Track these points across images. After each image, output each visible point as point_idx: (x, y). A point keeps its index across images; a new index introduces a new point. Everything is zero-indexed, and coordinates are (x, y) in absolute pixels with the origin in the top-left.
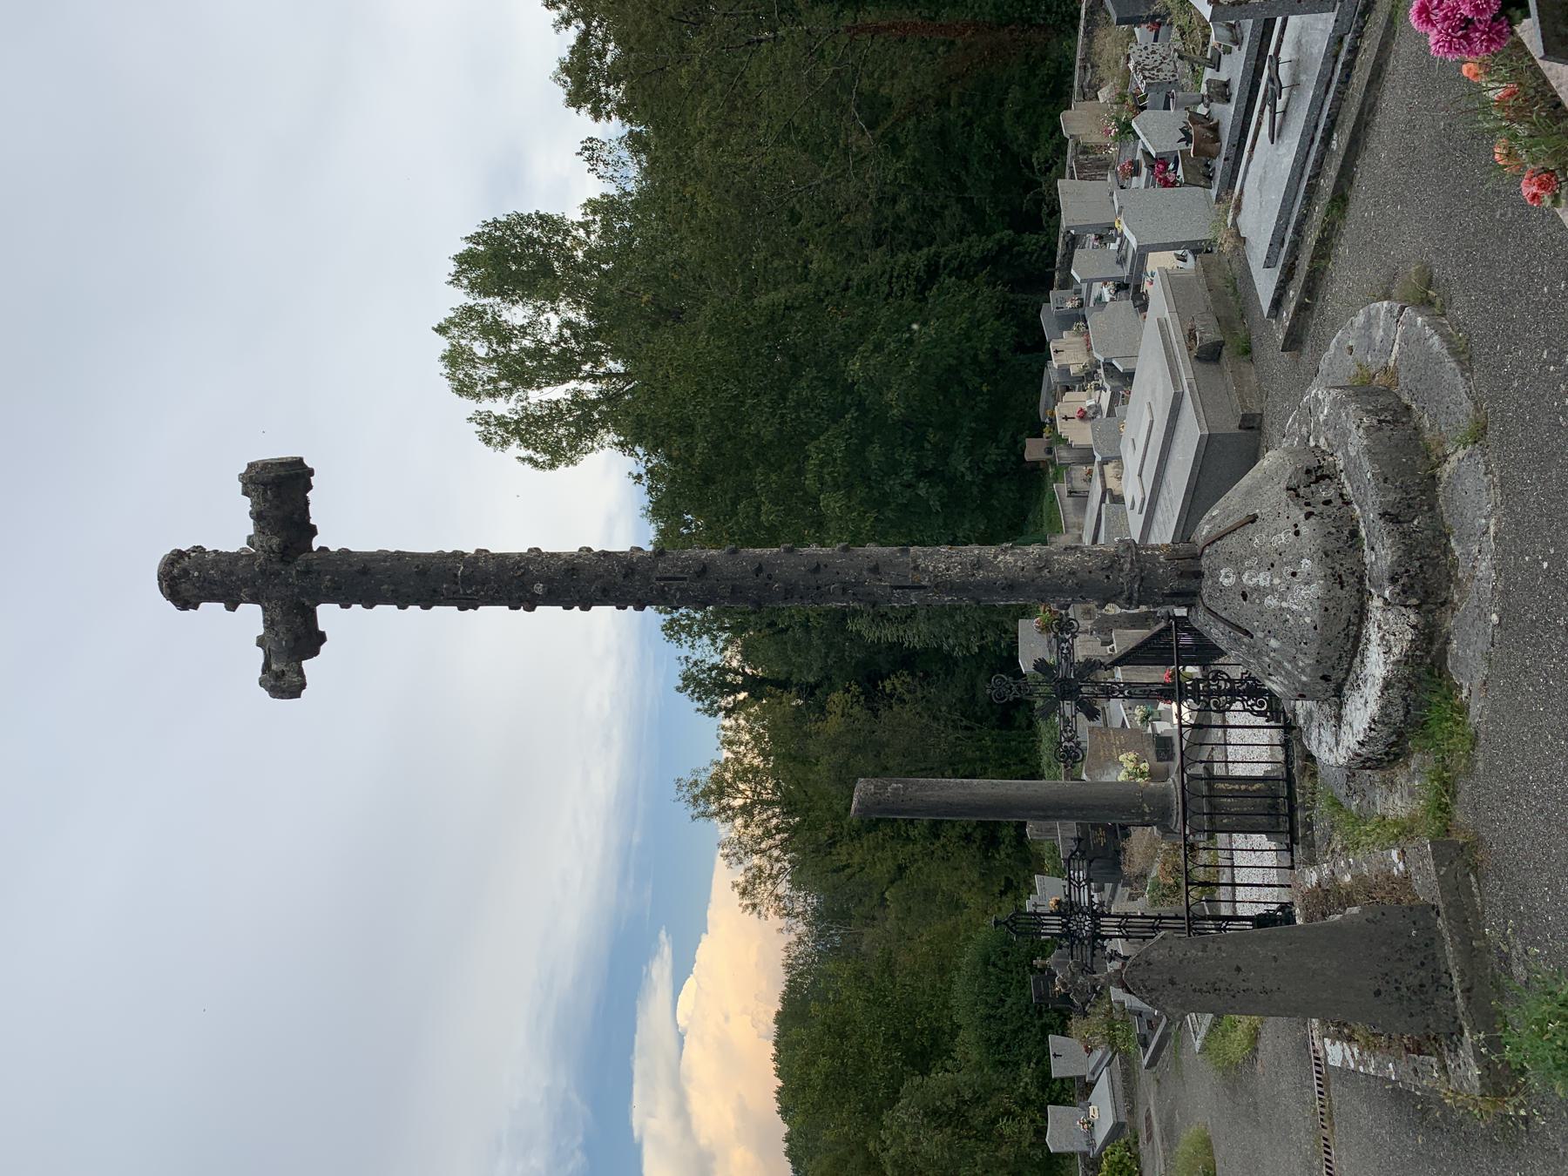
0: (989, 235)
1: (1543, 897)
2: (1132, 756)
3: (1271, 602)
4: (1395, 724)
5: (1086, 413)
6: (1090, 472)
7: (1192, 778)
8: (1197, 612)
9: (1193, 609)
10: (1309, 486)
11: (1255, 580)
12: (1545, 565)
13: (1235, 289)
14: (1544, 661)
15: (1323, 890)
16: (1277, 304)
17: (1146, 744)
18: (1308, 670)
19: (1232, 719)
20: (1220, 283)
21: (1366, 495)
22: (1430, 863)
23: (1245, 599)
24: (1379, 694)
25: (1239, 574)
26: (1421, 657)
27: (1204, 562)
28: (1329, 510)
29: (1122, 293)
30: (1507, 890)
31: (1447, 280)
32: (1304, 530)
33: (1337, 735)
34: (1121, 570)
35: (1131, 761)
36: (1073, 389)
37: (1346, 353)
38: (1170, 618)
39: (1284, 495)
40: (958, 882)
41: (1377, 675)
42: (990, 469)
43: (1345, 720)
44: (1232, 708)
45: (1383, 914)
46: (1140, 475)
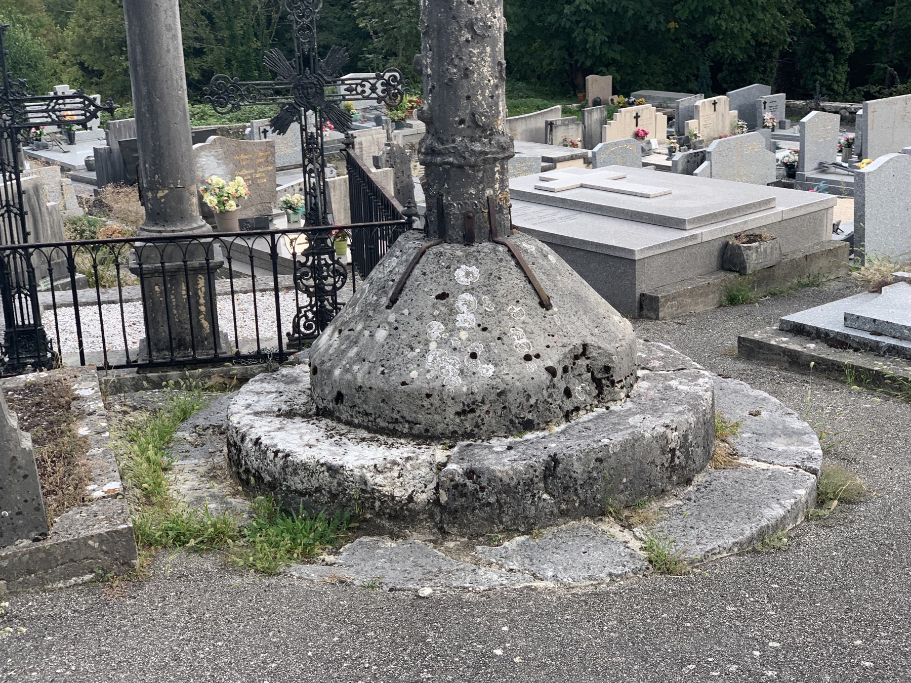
0: (850, 25)
1: (62, 664)
2: (243, 191)
3: (436, 329)
4: (285, 480)
5: (643, 138)
6: (574, 145)
7: (208, 248)
8: (418, 239)
9: (421, 236)
10: (588, 371)
11: (464, 309)
12: (499, 652)
13: (807, 285)
14: (373, 655)
15: (68, 403)
16: (799, 330)
17: (259, 207)
18: (349, 376)
19: (288, 301)
20: (814, 269)
21: (579, 438)
22: (103, 528)
23: (438, 297)
24: (322, 461)
25: (471, 290)
26: (373, 508)
27: (487, 246)
28: (559, 395)
29: (783, 171)
30: (73, 619)
31: (852, 522)
32: (533, 367)
33: (268, 413)
34: (472, 140)
35: (237, 191)
36: (670, 126)
37: (751, 408)
38: (410, 216)
39: (577, 341)
40: (87, 13)
41: (346, 458)
42: (578, 35)
43: (288, 423)
44: (299, 292)
45: (25, 477)
46: (582, 186)
